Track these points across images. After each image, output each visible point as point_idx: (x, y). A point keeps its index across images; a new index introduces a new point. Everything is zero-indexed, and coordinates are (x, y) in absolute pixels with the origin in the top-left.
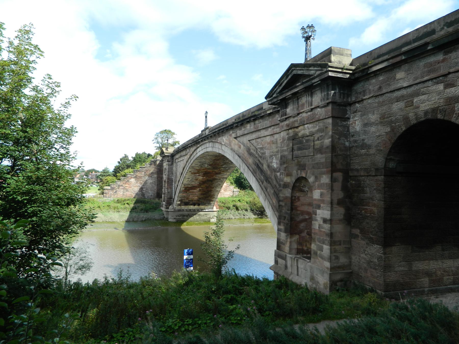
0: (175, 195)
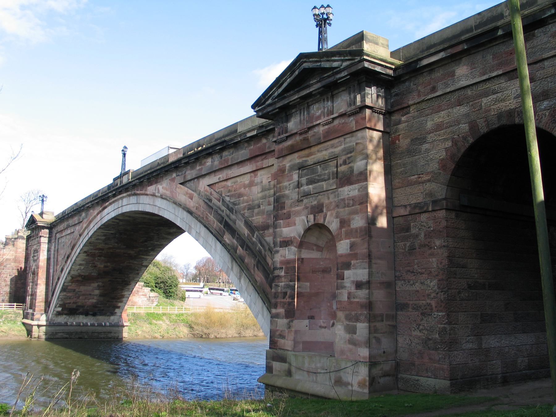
0: (53, 295)
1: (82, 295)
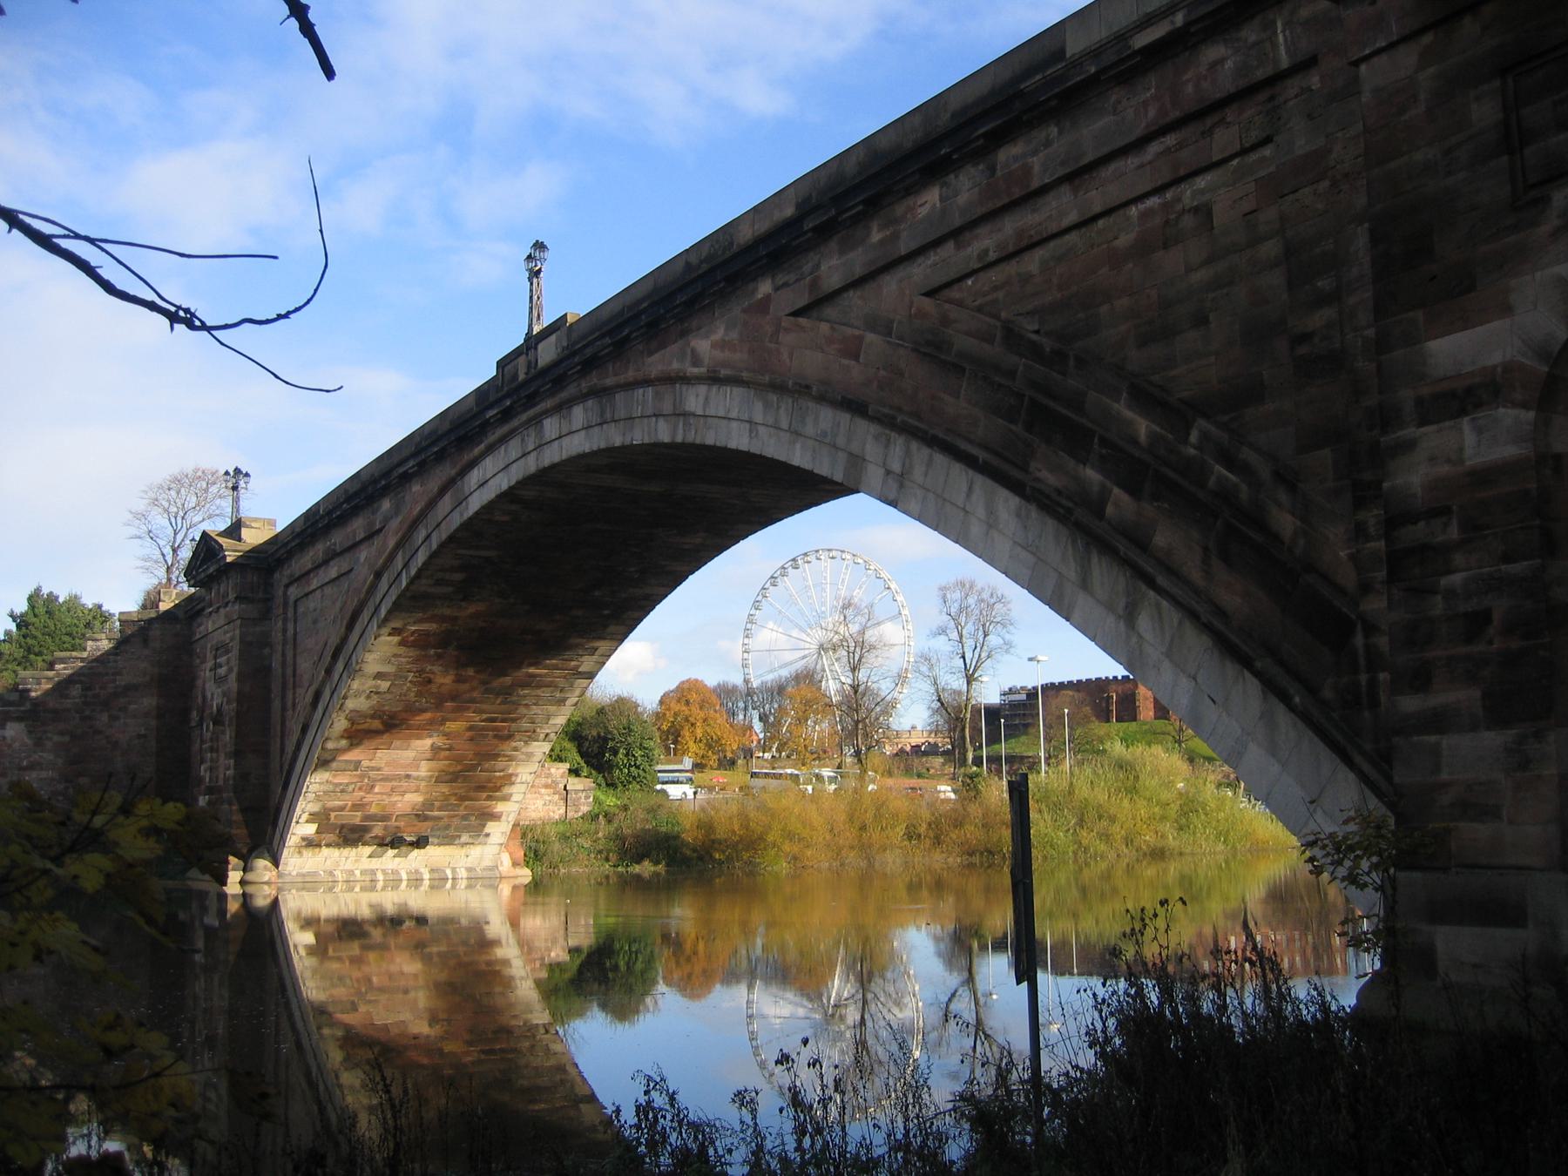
1: (381, 780)
